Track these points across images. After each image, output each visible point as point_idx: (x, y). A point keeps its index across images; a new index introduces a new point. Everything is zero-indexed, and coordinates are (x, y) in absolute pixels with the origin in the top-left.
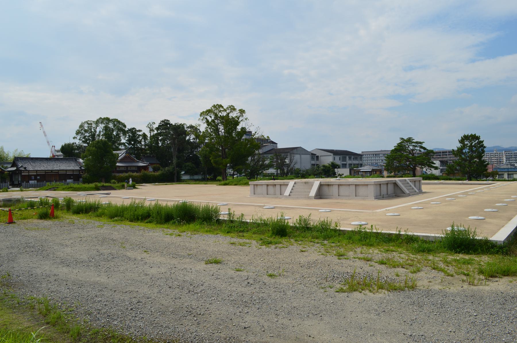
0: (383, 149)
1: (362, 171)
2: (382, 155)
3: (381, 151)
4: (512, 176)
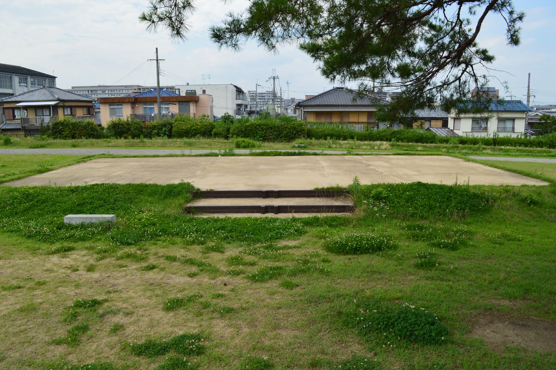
0: (102, 84)
1: (26, 108)
2: (101, 92)
3: (100, 86)
4: (509, 125)
